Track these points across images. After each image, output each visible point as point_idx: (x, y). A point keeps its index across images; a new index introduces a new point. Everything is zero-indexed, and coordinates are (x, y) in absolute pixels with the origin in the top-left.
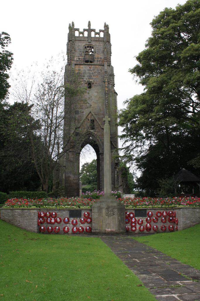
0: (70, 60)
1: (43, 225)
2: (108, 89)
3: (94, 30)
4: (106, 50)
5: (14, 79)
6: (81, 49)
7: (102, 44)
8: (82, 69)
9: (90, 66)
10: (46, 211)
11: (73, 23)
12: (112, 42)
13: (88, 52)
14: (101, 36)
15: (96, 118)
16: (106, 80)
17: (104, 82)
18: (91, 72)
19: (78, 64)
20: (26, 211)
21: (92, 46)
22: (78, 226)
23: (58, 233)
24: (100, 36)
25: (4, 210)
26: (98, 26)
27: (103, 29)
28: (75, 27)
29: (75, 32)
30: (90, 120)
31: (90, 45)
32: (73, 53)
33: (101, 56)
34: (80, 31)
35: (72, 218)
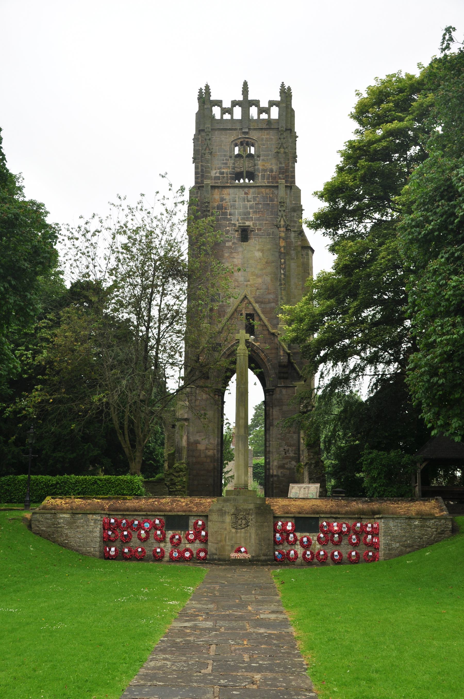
0: (200, 174)
1: (114, 544)
2: (286, 242)
3: (256, 103)
4: (282, 150)
5: (62, 241)
6: (225, 151)
7: (272, 136)
8: (227, 197)
9: (246, 190)
10: (120, 517)
11: (207, 87)
12: (298, 129)
13: (240, 148)
14: (272, 117)
15: (259, 312)
16: (282, 223)
17: (278, 227)
18: (248, 204)
19: (218, 187)
20: (80, 516)
21: (253, 141)
22: (182, 547)
23: (141, 558)
24: (269, 116)
25: (38, 515)
26: (265, 93)
27: (278, 98)
28: (212, 98)
29: (213, 108)
30: (244, 315)
31: (246, 140)
32: (207, 161)
33: (271, 164)
34: (224, 106)
35: (170, 532)
